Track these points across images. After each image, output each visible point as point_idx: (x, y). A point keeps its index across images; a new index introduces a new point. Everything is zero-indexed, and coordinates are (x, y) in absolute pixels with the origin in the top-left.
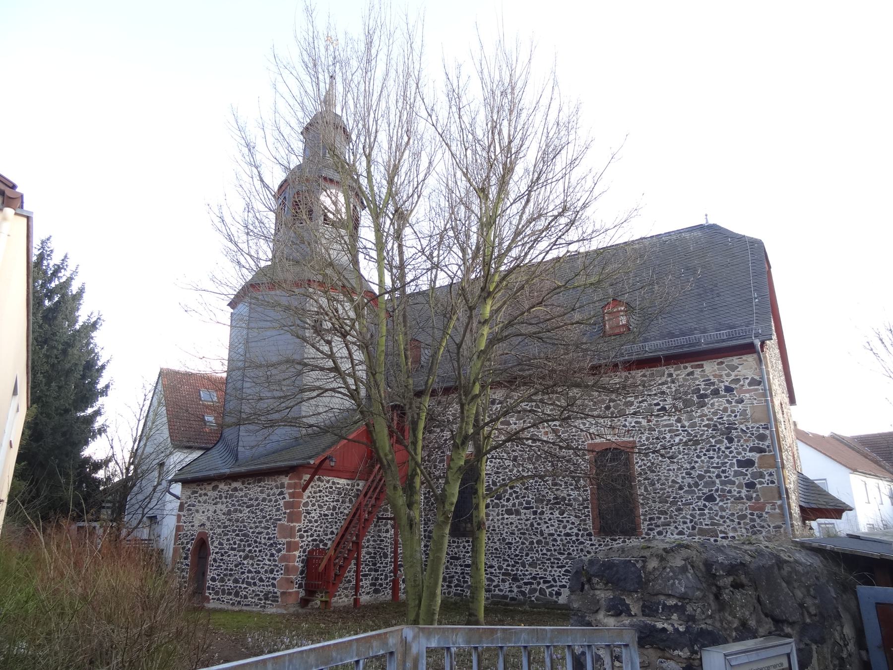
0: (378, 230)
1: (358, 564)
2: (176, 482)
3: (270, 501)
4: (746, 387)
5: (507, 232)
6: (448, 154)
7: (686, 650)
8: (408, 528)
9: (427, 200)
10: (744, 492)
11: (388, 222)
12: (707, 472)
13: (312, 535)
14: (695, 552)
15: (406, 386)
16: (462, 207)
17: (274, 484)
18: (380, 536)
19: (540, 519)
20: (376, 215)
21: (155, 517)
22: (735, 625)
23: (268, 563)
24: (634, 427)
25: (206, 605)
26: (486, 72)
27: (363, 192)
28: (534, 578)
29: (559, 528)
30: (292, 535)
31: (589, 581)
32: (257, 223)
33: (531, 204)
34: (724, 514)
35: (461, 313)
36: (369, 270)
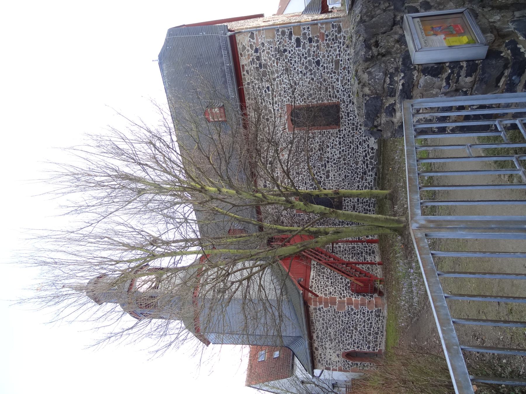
0: (163, 255)
1: (359, 263)
2: (313, 373)
3: (324, 316)
4: (255, 41)
5: (166, 177)
6: (116, 213)
7: (414, 73)
8: (339, 235)
9: (144, 226)
10: (314, 44)
11: (158, 249)
12: (303, 64)
14: (359, 67)
15: (258, 237)
16: (149, 204)
17: (314, 314)
18: (343, 251)
19: (331, 159)
20: (154, 256)
21: (333, 384)
22: (398, 46)
23: (359, 316)
24: (278, 105)
26: (64, 191)
27: (140, 265)
28: (364, 162)
29: (336, 148)
30: (343, 302)
31: (376, 127)
32: (159, 330)
33: (147, 163)
34: (326, 56)
35: (214, 204)
36: (188, 260)
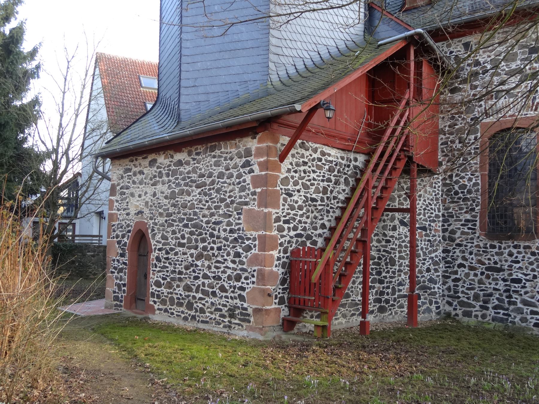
3: (231, 176)
13: (295, 228)
17: (234, 151)
18: (385, 235)
23: (231, 265)
25: (150, 316)
30: (266, 227)
